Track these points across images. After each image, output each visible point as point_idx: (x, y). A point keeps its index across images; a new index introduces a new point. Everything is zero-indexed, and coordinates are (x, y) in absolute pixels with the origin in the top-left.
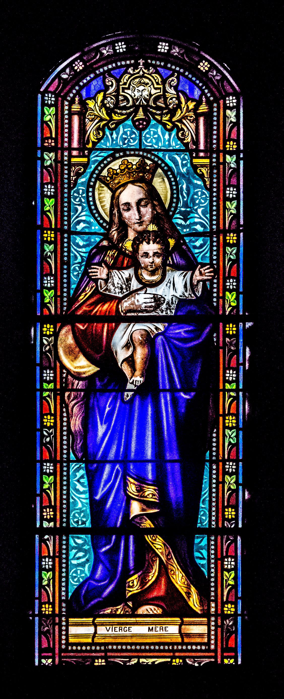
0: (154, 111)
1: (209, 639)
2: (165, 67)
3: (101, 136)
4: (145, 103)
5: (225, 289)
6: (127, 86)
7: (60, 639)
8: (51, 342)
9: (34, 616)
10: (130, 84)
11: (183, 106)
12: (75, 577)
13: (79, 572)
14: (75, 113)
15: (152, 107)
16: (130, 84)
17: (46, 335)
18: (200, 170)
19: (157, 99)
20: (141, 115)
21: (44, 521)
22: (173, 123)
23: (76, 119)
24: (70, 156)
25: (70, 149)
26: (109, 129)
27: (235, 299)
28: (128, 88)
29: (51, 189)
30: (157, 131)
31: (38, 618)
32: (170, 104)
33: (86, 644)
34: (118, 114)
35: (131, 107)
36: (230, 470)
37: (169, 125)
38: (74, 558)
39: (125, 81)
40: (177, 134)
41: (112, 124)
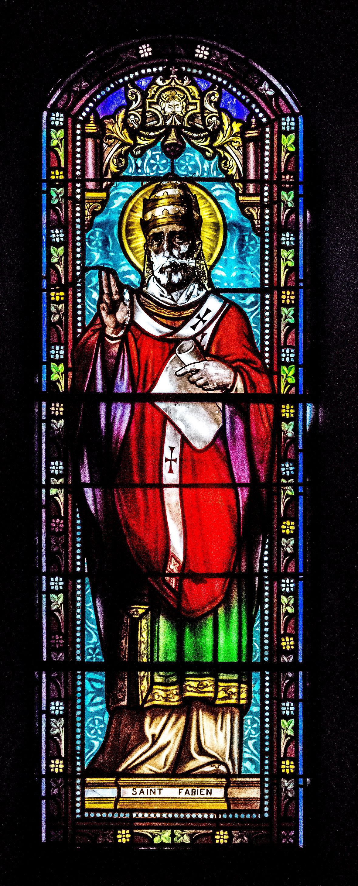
0: (189, 133)
1: (262, 806)
2: (203, 77)
3: (123, 165)
4: (178, 123)
5: (281, 305)
6: (155, 100)
7: (75, 322)
8: (60, 193)
9: (41, 712)
10: (159, 97)
11: (226, 127)
12: (92, 729)
13: (97, 722)
14: (91, 135)
15: (186, 128)
16: (159, 97)
17: (55, 302)
18: (247, 210)
19: (192, 118)
20: (172, 138)
21: (52, 363)
22: (214, 149)
23: (90, 143)
24: (84, 189)
25: (83, 180)
26: (133, 155)
27: (293, 143)
28: (157, 103)
29: (59, 706)
30: (194, 155)
31: (46, 366)
32: (210, 124)
33: (107, 811)
34: (144, 136)
35: (161, 127)
36: (288, 359)
37: (209, 152)
38: (91, 705)
39: (153, 93)
40: (220, 165)
41: (136, 150)
